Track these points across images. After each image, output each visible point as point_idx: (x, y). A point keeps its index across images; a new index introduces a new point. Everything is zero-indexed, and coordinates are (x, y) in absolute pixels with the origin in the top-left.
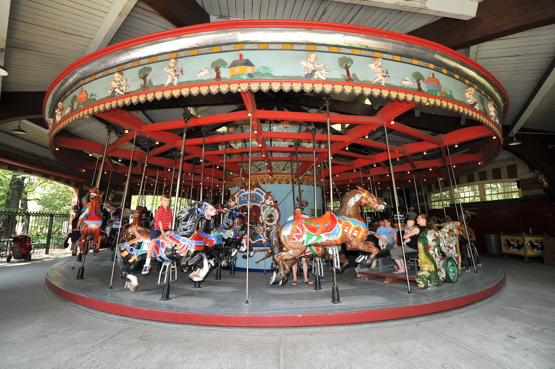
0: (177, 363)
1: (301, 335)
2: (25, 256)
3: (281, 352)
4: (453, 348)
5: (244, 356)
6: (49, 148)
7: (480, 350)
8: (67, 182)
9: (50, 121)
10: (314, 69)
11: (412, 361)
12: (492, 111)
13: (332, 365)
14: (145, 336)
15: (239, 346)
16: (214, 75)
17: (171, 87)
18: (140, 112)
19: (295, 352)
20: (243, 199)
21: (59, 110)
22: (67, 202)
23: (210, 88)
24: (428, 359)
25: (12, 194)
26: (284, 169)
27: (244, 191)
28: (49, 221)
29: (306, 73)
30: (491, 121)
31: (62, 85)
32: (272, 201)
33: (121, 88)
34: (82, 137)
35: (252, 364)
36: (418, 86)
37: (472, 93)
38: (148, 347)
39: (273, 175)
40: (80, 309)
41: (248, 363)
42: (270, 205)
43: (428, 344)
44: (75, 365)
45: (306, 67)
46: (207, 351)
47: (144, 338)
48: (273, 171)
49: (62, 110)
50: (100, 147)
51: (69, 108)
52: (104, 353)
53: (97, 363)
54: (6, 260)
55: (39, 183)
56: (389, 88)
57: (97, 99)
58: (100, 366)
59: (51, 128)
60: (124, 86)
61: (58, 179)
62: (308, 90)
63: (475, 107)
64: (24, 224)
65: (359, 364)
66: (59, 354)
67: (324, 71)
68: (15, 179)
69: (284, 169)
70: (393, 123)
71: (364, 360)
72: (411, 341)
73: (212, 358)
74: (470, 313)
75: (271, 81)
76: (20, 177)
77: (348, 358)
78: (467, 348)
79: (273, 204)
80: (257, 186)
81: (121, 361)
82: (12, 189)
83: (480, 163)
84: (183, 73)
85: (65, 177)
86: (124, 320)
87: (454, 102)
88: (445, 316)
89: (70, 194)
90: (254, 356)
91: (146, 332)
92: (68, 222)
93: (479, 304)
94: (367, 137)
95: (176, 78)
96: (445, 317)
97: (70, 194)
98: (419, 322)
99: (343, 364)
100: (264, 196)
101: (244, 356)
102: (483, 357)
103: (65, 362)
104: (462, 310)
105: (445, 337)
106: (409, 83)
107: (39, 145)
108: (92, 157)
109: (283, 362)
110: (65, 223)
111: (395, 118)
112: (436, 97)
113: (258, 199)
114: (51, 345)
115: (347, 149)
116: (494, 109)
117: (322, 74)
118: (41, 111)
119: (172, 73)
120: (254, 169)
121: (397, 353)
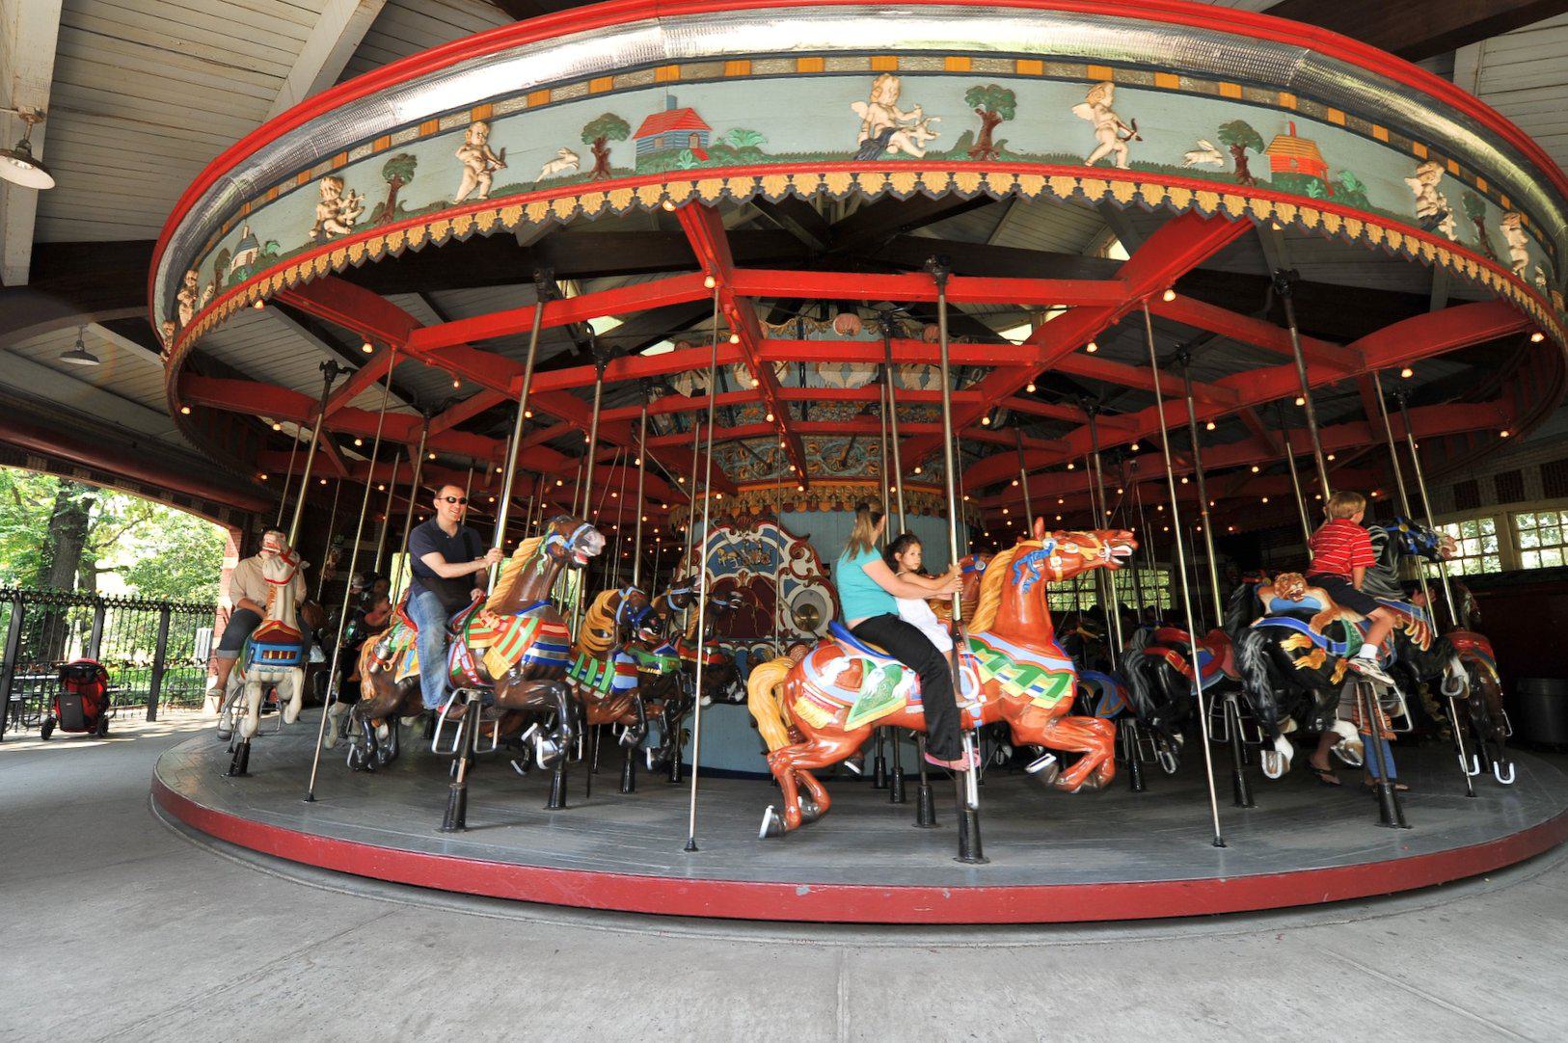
0: (528, 1009)
1: (903, 950)
2: (93, 724)
3: (840, 993)
4: (1397, 1003)
5: (726, 999)
6: (169, 412)
7: (1491, 1013)
8: (210, 511)
9: (164, 329)
10: (890, 124)
11: (1259, 1034)
12: (1514, 241)
13: (999, 1034)
14: (431, 935)
15: (712, 973)
16: (590, 162)
17: (470, 206)
18: (416, 297)
19: (884, 995)
20: (724, 559)
21: (186, 293)
22: (209, 573)
23: (1020, 180)
24: (1315, 1032)
25: (57, 548)
26: (844, 464)
27: (728, 535)
28: (157, 627)
29: (864, 137)
30: (1515, 281)
31: (206, 207)
32: (813, 565)
33: (341, 218)
34: (254, 377)
35: (753, 1021)
36: (1238, 165)
37: (1435, 181)
38: (443, 964)
39: (811, 483)
40: (248, 861)
41: (739, 1016)
42: (805, 578)
43: (1317, 990)
44: (236, 1001)
45: (865, 121)
46: (615, 982)
47: (431, 940)
48: (810, 469)
49: (195, 293)
50: (302, 408)
51: (210, 288)
52: (316, 974)
53: (296, 998)
54: (39, 734)
55: (129, 523)
56: (1140, 173)
57: (280, 252)
58: (306, 1007)
59: (169, 349)
60: (348, 211)
61: (181, 501)
62: (935, 191)
63: (1442, 228)
64: (87, 634)
65: (1086, 1036)
66: (190, 972)
67: (921, 134)
68: (64, 506)
69: (844, 464)
70: (1170, 296)
71: (1102, 1024)
72: (1258, 981)
73: (632, 999)
74: (1460, 910)
75: (791, 171)
76: (78, 499)
77: (1052, 1019)
78: (1447, 1005)
79: (816, 573)
80: (767, 516)
81: (366, 995)
82: (56, 534)
83: (1504, 434)
84: (507, 160)
85: (205, 495)
86: (372, 893)
87: (1367, 215)
88: (1373, 914)
89: (218, 548)
90: (758, 999)
91: (436, 925)
92: (210, 630)
93: (1489, 884)
94: (1092, 348)
95: (484, 179)
96: (1373, 918)
97: (218, 548)
98: (1287, 927)
99: (1034, 1033)
100: (788, 547)
101: (726, 999)
102: (1501, 1033)
103: (209, 992)
104: (1432, 901)
105: (1373, 972)
106: (1212, 158)
107: (132, 400)
108: (280, 432)
109: (847, 1020)
110: (203, 632)
111: (1178, 281)
112: (1301, 201)
113: (771, 557)
114: (169, 948)
115: (1031, 388)
116: (1525, 240)
117: (914, 141)
118: (144, 299)
119: (476, 165)
120: (752, 465)
121: (1212, 1012)
